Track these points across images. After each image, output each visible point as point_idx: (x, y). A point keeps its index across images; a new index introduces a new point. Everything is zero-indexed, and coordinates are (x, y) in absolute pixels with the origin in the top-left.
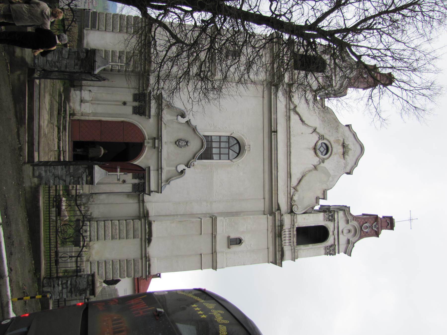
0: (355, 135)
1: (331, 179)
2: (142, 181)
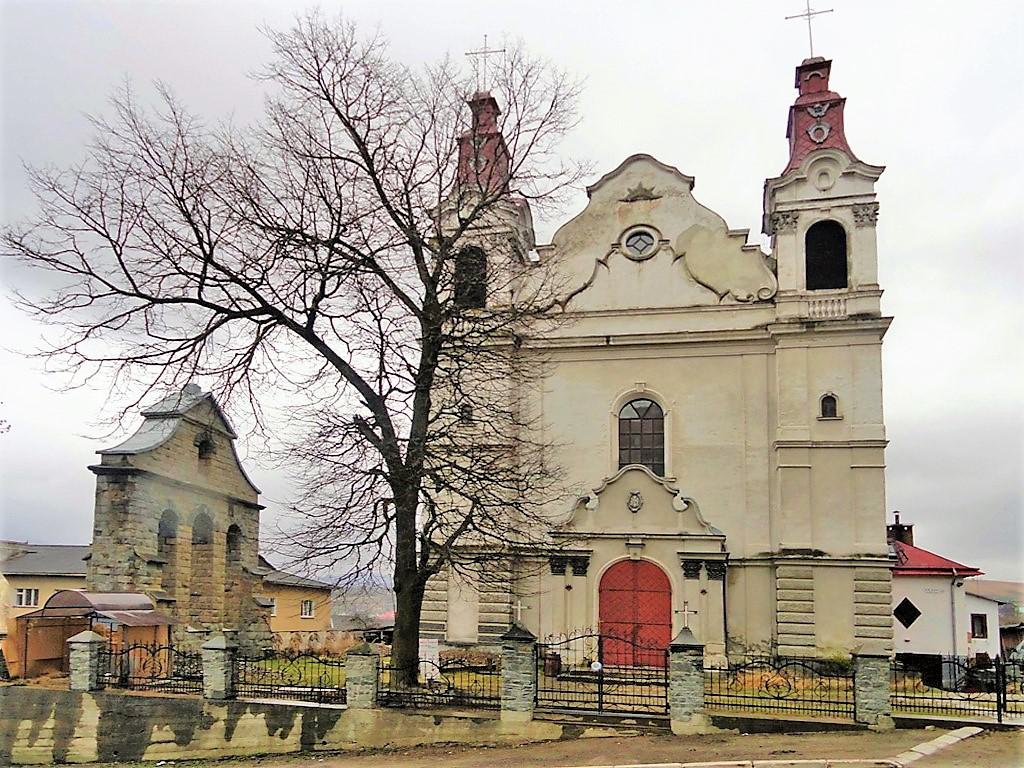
0: (607, 178)
1: (703, 224)
2: (703, 564)
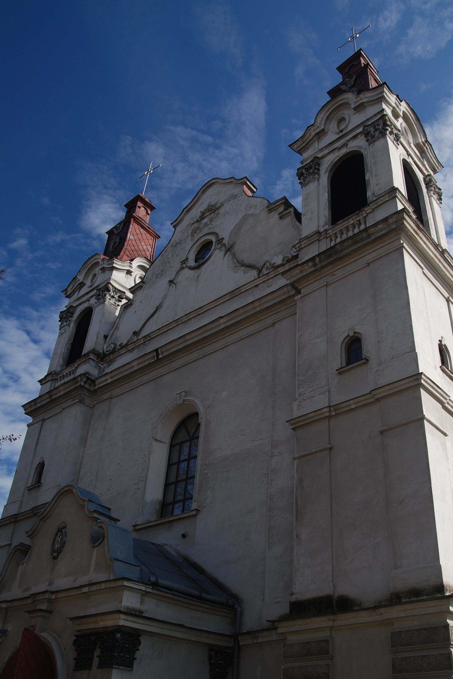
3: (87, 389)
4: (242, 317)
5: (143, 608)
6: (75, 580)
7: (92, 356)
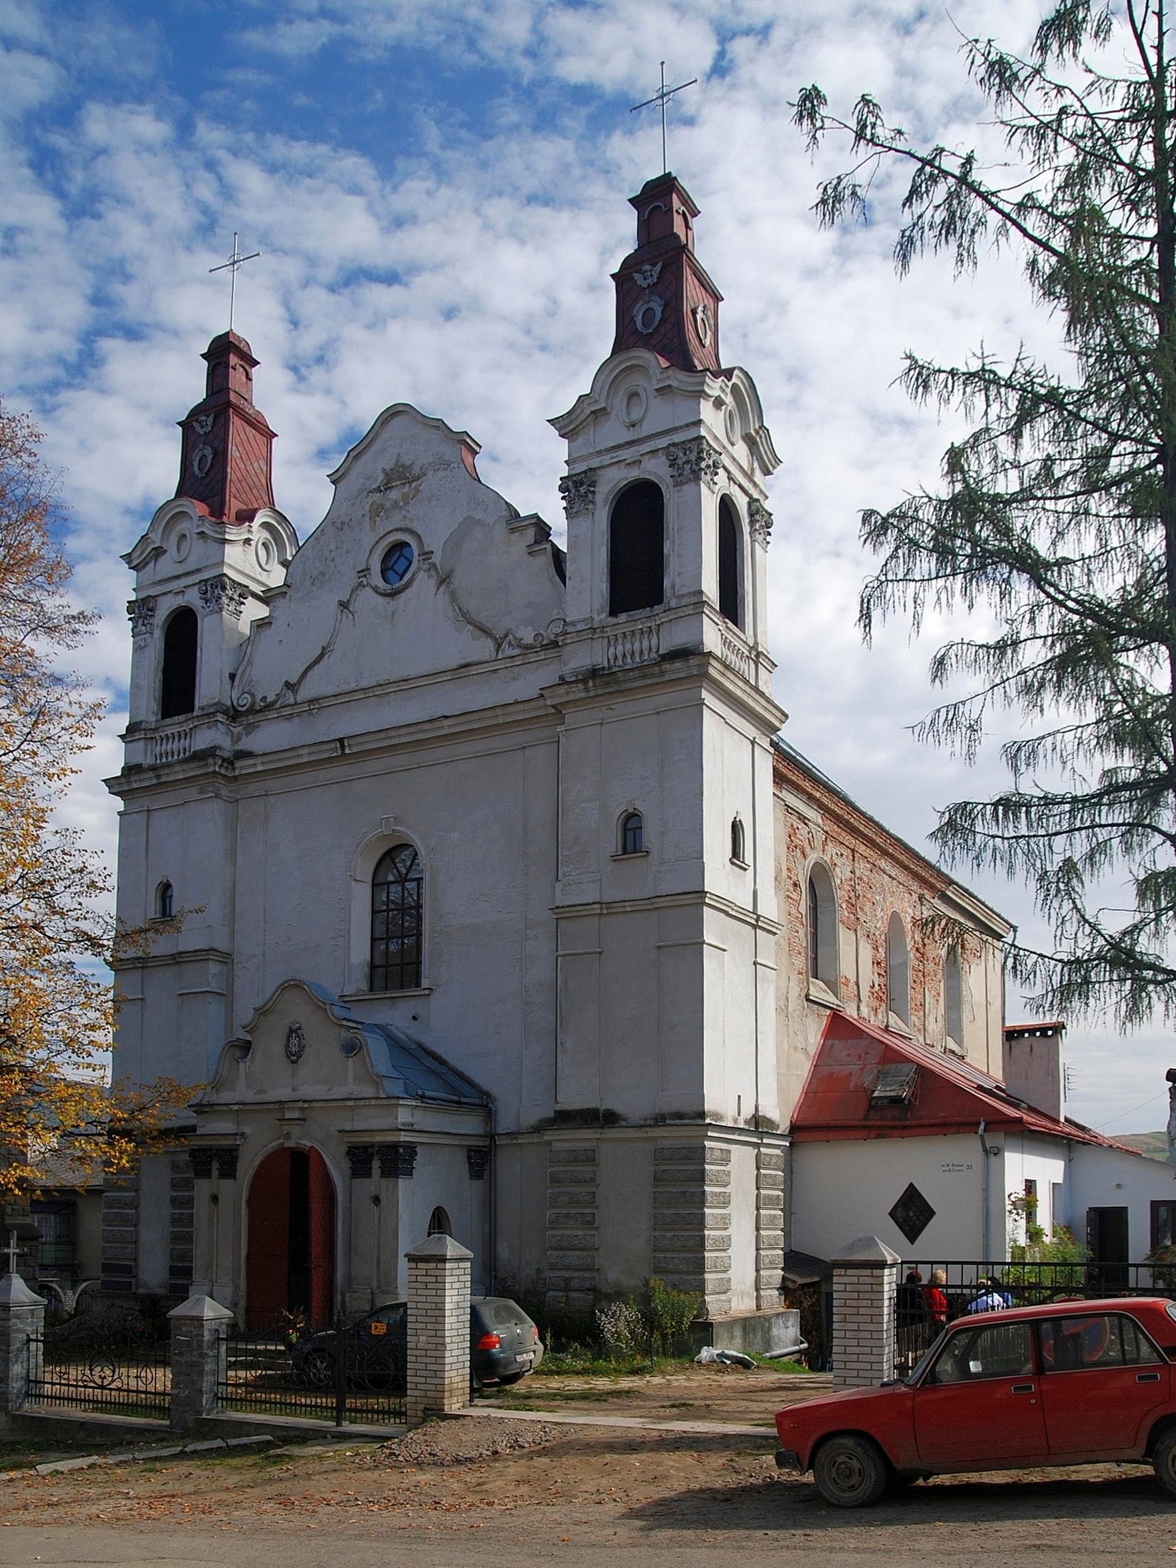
1: (478, 515)
3: (222, 775)
4: (477, 726)
5: (413, 1121)
6: (329, 1090)
7: (220, 717)
